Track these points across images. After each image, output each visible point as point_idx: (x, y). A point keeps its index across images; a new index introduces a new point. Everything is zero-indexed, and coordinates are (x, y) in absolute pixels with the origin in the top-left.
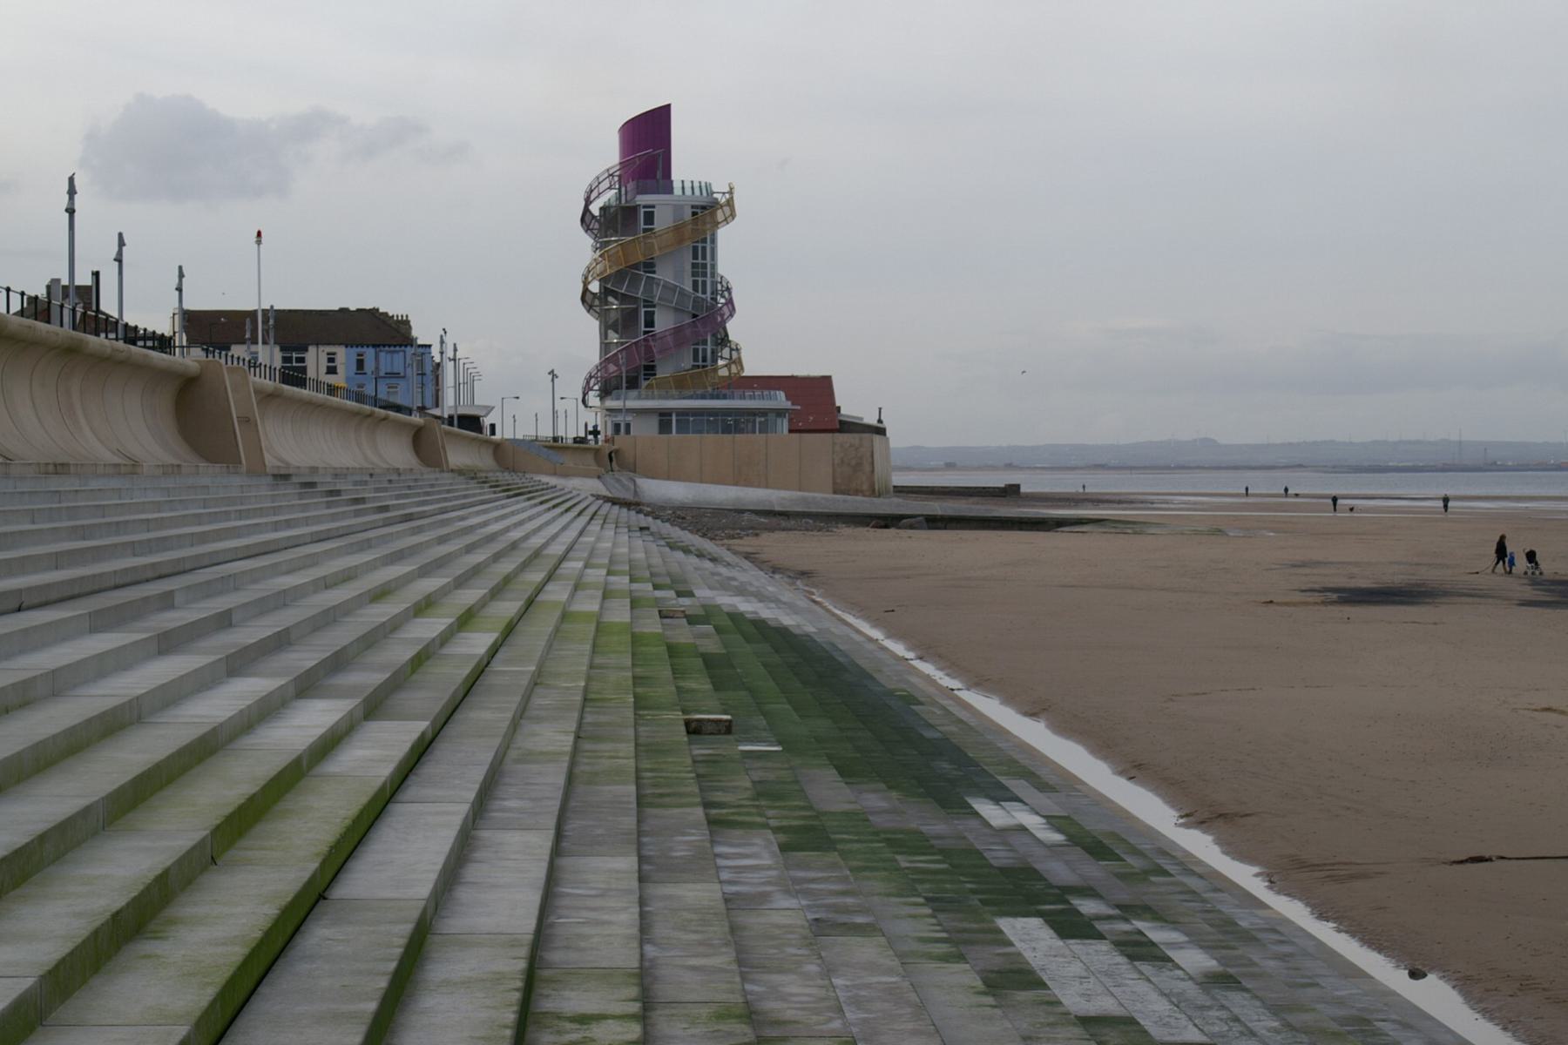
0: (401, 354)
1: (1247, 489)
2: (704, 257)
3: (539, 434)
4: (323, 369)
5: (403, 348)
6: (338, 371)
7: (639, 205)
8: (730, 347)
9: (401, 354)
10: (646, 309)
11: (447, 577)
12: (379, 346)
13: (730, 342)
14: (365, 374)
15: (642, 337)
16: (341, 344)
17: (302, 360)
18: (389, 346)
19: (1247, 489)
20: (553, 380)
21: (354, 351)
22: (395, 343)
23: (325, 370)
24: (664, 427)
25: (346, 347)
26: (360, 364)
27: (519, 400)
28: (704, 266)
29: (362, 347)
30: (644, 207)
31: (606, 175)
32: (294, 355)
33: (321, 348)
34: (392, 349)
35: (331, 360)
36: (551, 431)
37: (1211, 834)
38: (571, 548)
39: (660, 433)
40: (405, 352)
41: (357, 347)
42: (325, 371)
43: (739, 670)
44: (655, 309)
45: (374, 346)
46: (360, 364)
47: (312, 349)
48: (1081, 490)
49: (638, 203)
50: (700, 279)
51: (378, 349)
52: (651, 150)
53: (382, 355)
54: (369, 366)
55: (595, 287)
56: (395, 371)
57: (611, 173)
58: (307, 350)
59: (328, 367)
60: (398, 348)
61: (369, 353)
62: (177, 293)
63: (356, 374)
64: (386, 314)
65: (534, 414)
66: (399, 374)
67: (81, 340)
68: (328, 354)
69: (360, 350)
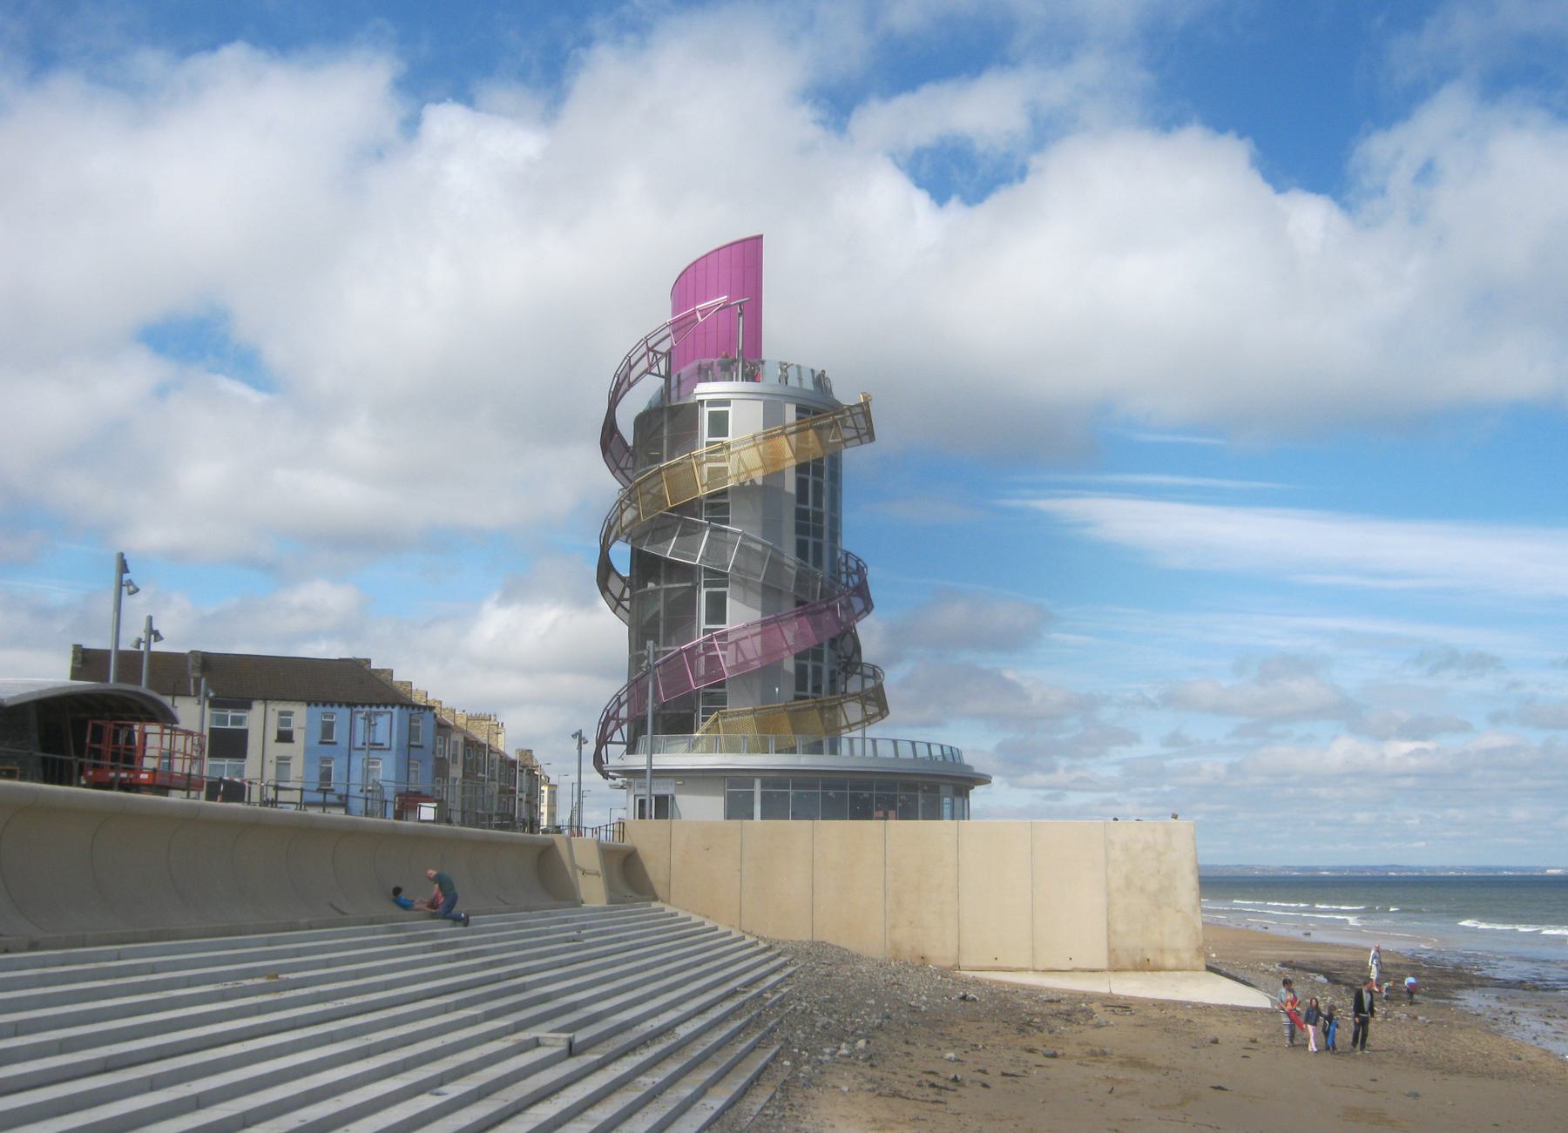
0: (387, 717)
2: (818, 503)
3: (263, 706)
4: (272, 735)
5: (389, 709)
6: (295, 737)
7: (702, 402)
8: (861, 673)
9: (387, 717)
10: (709, 589)
11: (599, 1053)
12: (355, 705)
13: (860, 664)
14: (335, 743)
15: (702, 638)
18: (371, 705)
20: (580, 745)
22: (378, 702)
23: (275, 736)
24: (738, 809)
25: (309, 705)
26: (328, 730)
28: (819, 517)
29: (332, 706)
30: (712, 403)
31: (644, 349)
36: (110, 633)
38: (726, 1018)
39: (729, 816)
40: (391, 713)
41: (324, 705)
42: (275, 738)
44: (728, 590)
46: (328, 730)
47: (258, 707)
48: (651, 1029)
49: (699, 398)
50: (811, 540)
51: (355, 710)
52: (740, 348)
54: (339, 734)
55: (621, 556)
56: (378, 741)
57: (650, 345)
60: (382, 709)
61: (341, 715)
63: (321, 743)
65: (1212, 1090)
66: (382, 744)
69: (328, 709)
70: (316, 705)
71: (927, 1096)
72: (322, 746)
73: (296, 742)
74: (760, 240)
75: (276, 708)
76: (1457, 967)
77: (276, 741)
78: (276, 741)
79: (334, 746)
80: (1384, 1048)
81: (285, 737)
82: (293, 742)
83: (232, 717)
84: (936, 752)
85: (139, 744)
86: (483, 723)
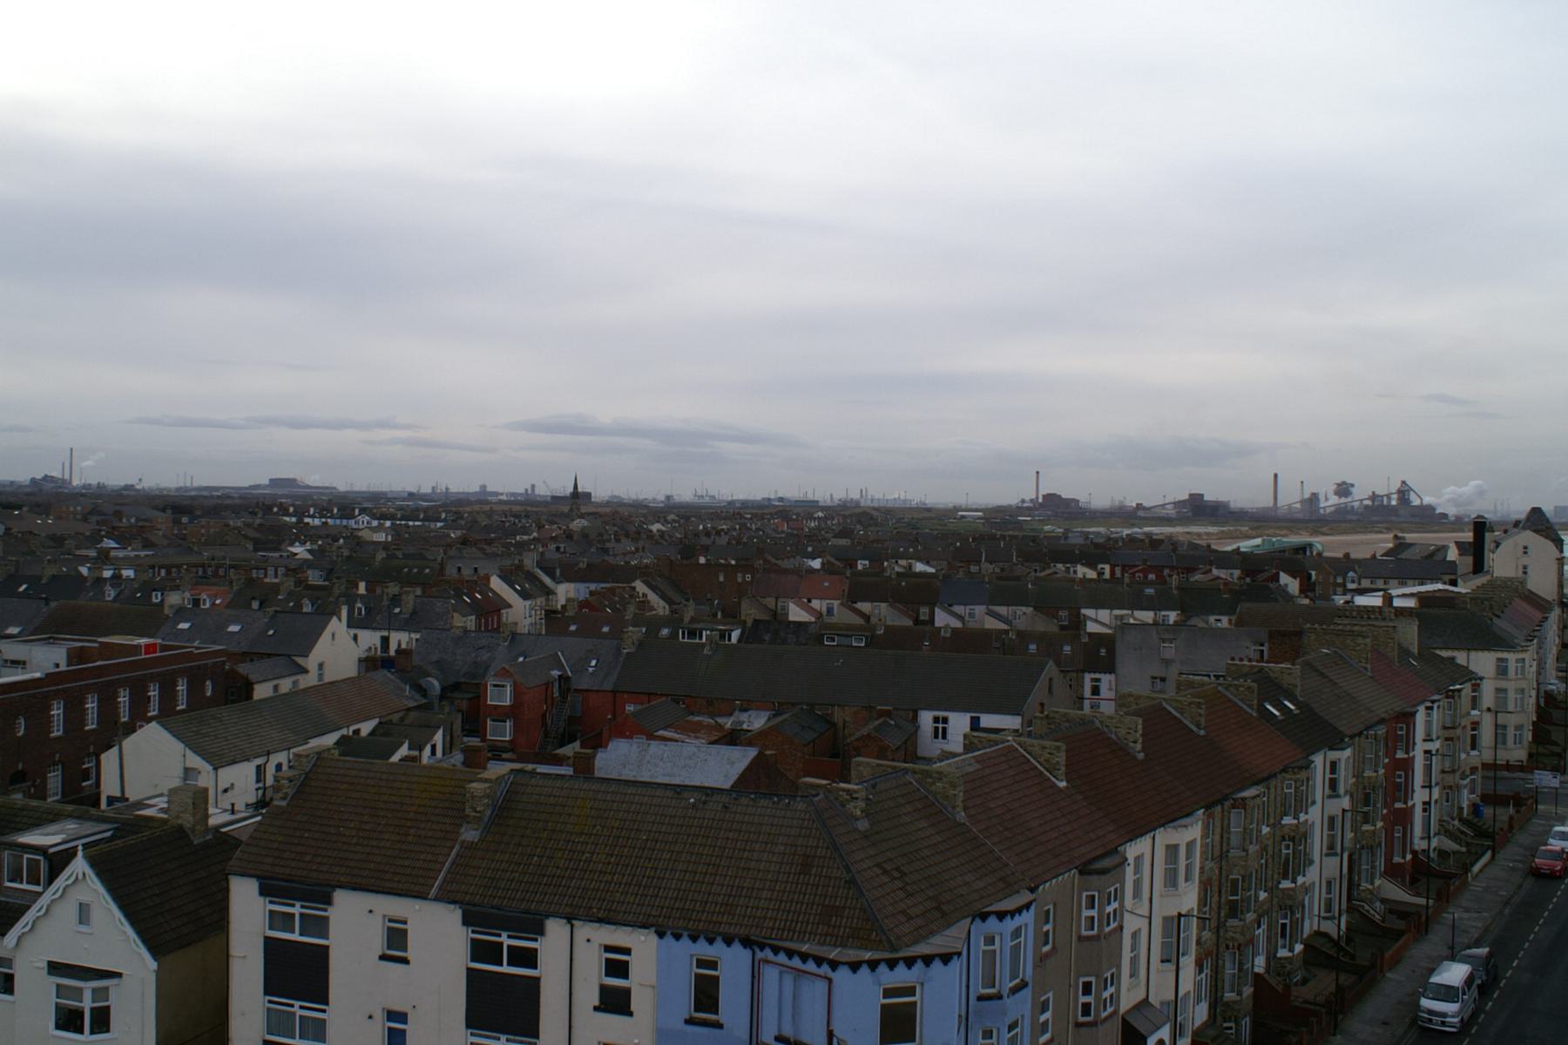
1: (233, 805)
4: (589, 995)
14: (718, 1025)
16: (644, 926)
17: (527, 958)
19: (233, 805)
21: (685, 952)
25: (661, 935)
26: (706, 995)
27: (1040, 470)
32: (506, 940)
33: (584, 930)
34: (796, 962)
35: (617, 968)
37: (452, 493)
43: (1225, 622)
45: (747, 943)
46: (706, 995)
47: (556, 929)
51: (760, 955)
53: (770, 975)
58: (541, 932)
59: (604, 990)
61: (733, 963)
62: (183, 758)
63: (690, 1021)
64: (33, 481)
67: (1048, 1009)
68: (608, 949)
69: (703, 949)
70: (677, 937)
71: (844, 591)
72: (691, 1029)
73: (892, 973)
74: (1165, 958)
75: (595, 938)
76: (263, 659)
77: (596, 1009)
78: (596, 1009)
79: (717, 1031)
80: (437, 631)
81: (615, 1002)
82: (630, 1014)
83: (509, 946)
84: (17, 726)
85: (1354, 904)
86: (1360, 640)
